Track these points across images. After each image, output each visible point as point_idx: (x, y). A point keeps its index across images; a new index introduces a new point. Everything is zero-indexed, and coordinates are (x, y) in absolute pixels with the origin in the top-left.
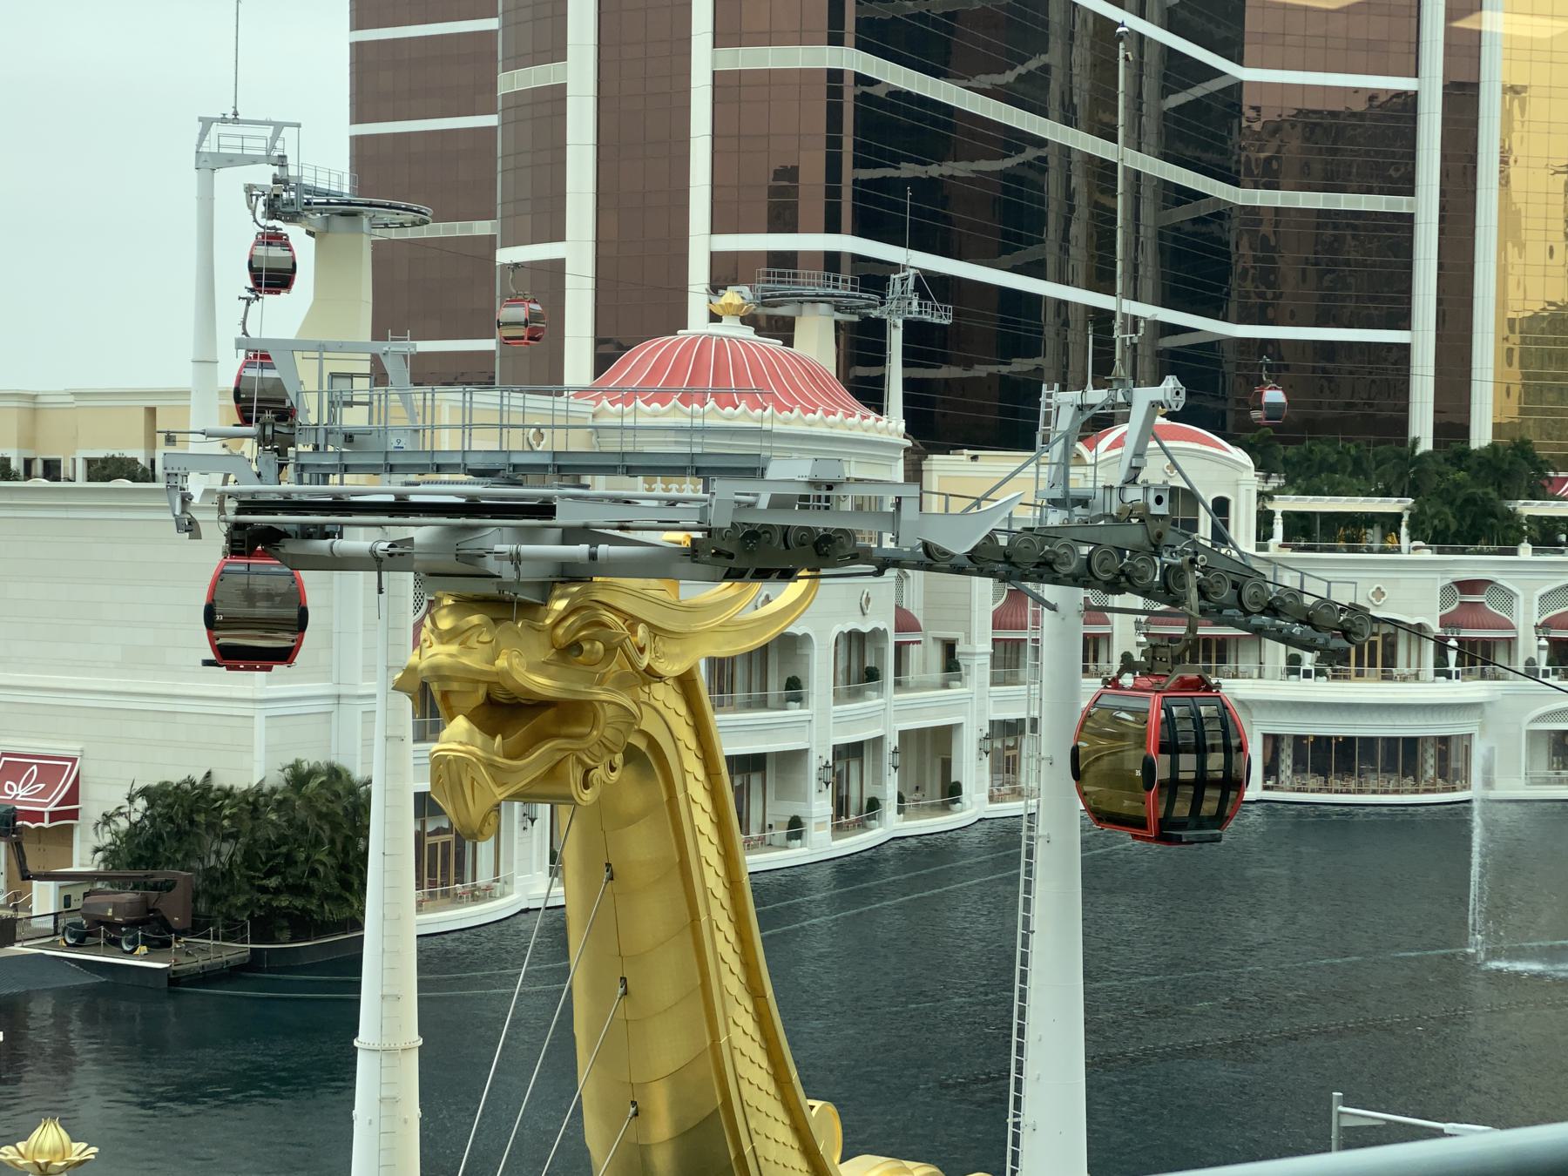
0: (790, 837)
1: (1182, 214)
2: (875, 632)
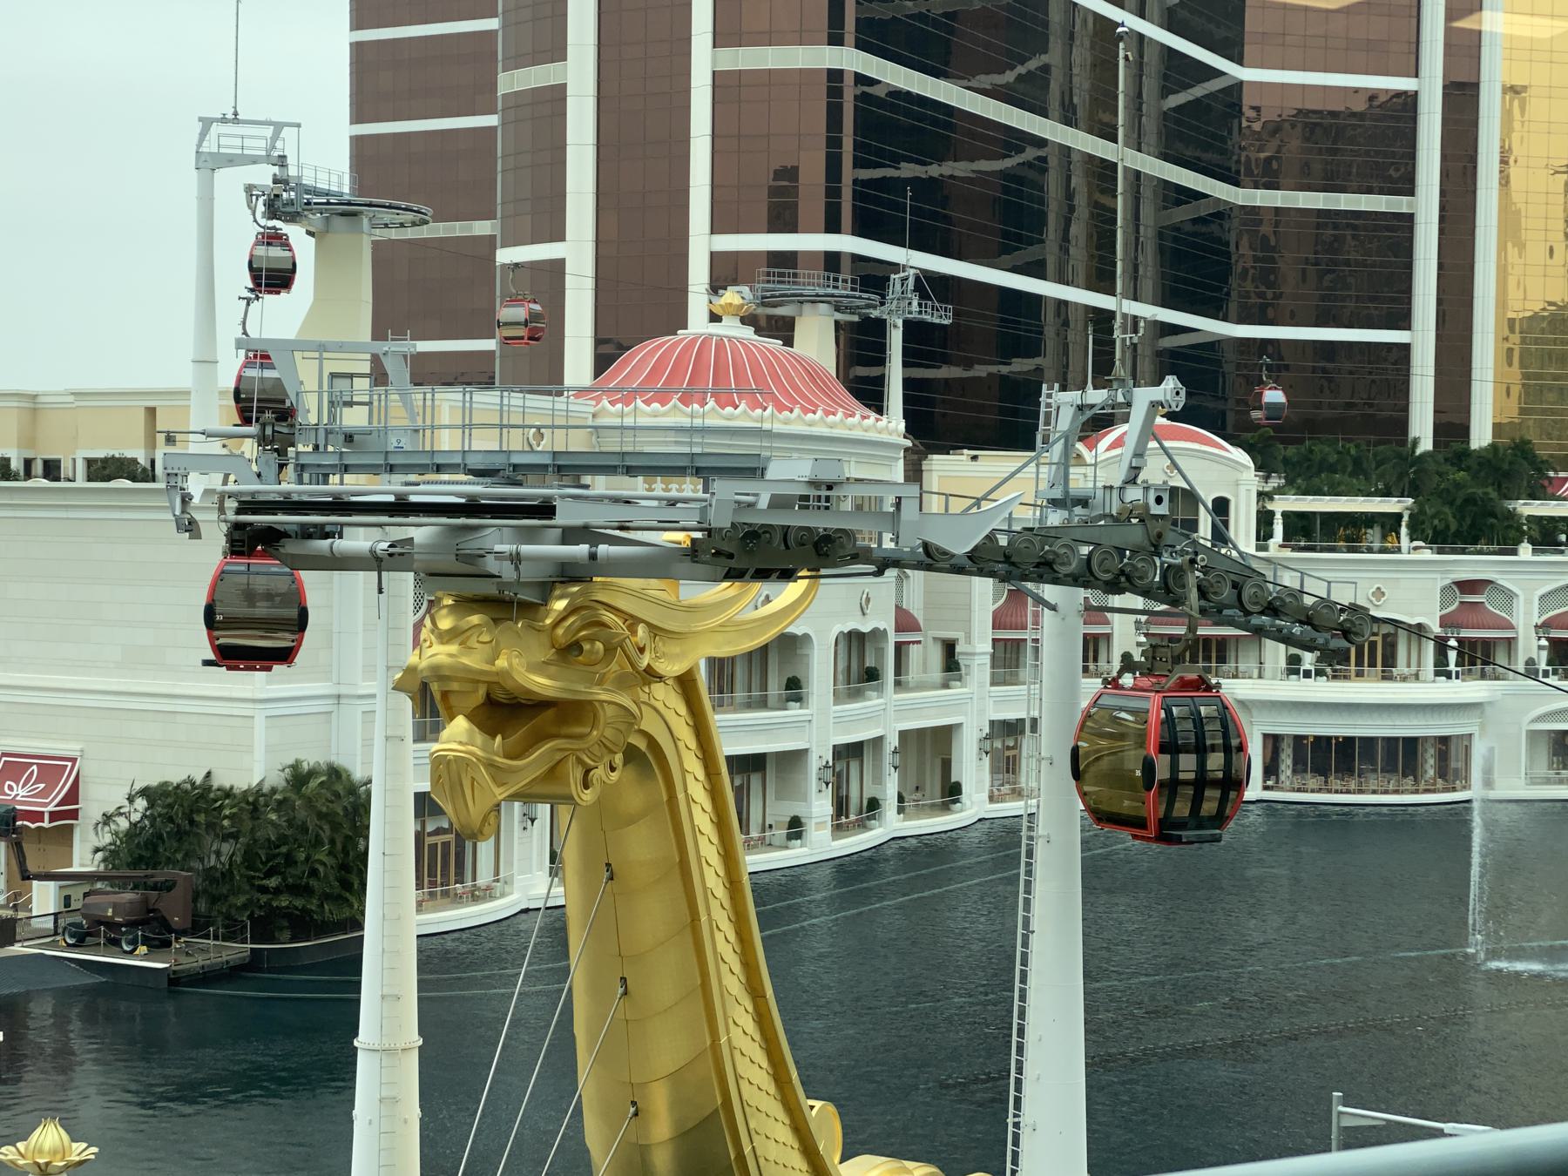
0: (790, 837)
1: (1182, 214)
2: (875, 632)
